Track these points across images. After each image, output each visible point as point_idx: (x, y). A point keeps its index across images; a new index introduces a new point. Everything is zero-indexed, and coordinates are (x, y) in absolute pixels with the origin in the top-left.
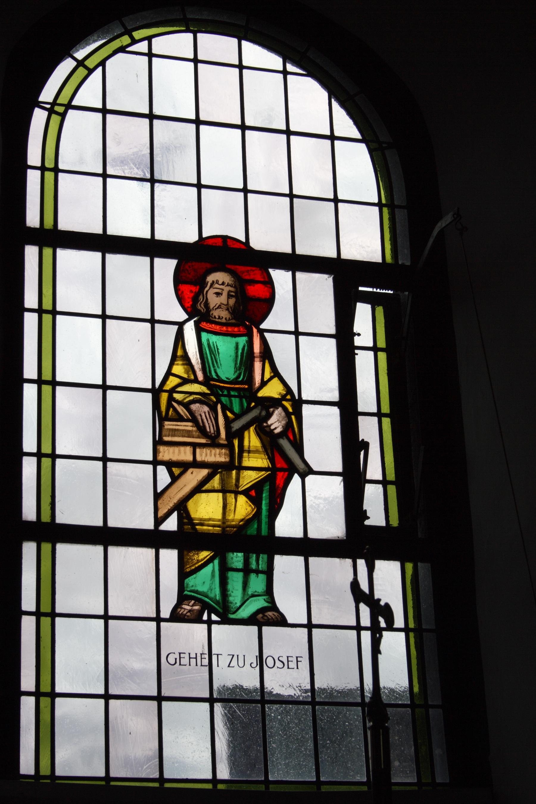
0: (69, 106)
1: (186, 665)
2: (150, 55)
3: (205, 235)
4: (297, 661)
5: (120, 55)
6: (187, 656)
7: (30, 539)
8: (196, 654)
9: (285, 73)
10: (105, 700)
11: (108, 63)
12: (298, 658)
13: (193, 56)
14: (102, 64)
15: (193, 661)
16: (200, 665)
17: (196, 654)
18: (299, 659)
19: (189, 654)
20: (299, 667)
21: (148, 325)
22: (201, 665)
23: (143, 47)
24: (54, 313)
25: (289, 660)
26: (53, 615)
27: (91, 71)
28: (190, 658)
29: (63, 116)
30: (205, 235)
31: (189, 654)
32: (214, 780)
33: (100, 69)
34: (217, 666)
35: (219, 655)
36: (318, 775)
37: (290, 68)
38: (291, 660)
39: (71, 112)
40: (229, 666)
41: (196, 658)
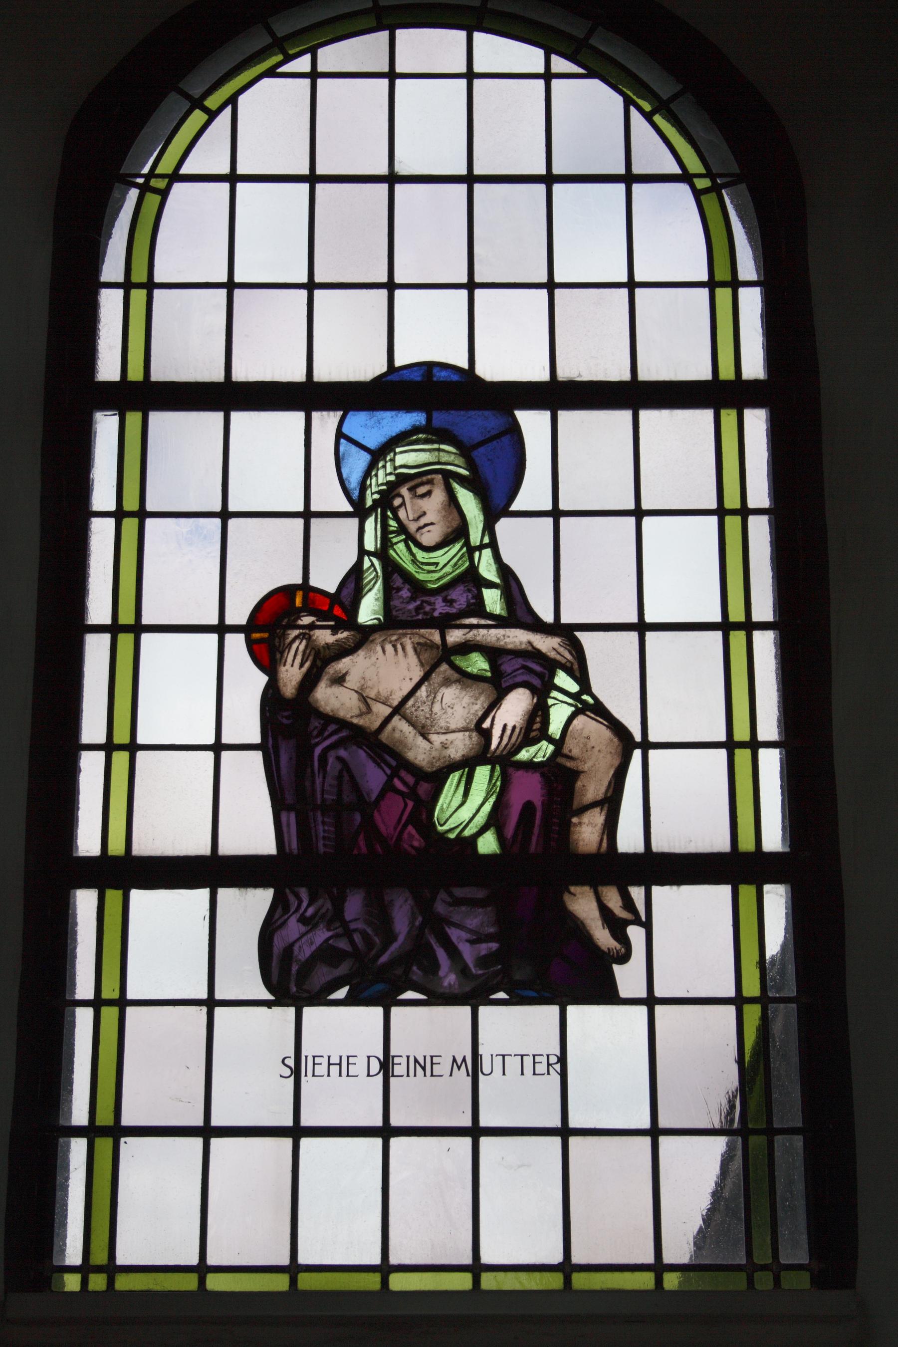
0: (176, 177)
1: (323, 1076)
2: (314, 75)
3: (399, 362)
4: (534, 1063)
5: (266, 81)
6: (324, 1061)
7: (86, 885)
8: (341, 1057)
9: (548, 76)
10: (203, 1139)
11: (242, 99)
12: (434, 1059)
13: (310, 69)
14: (233, 101)
15: (335, 1070)
16: (430, 1075)
17: (341, 1057)
18: (435, 1060)
19: (329, 1057)
20: (331, 1074)
21: (232, 523)
22: (348, 1075)
23: (303, 64)
24: (142, 514)
25: (434, 1061)
26: (122, 1003)
27: (212, 115)
28: (329, 1064)
29: (164, 194)
30: (399, 362)
31: (329, 1057)
32: (659, 1267)
33: (228, 111)
34: (338, 1075)
35: (506, 1057)
36: (749, 1254)
37: (560, 64)
38: (319, 1062)
39: (178, 188)
40: (369, 1075)
41: (340, 1064)
